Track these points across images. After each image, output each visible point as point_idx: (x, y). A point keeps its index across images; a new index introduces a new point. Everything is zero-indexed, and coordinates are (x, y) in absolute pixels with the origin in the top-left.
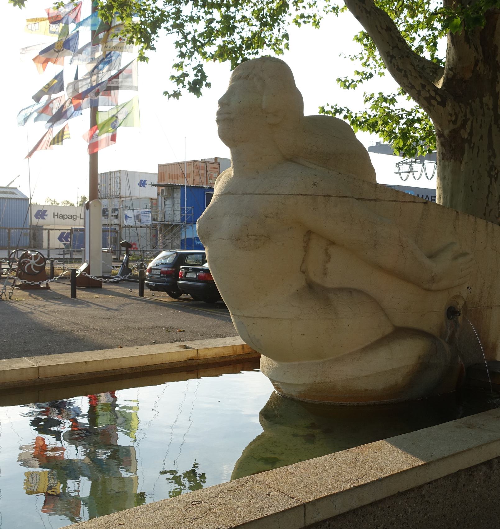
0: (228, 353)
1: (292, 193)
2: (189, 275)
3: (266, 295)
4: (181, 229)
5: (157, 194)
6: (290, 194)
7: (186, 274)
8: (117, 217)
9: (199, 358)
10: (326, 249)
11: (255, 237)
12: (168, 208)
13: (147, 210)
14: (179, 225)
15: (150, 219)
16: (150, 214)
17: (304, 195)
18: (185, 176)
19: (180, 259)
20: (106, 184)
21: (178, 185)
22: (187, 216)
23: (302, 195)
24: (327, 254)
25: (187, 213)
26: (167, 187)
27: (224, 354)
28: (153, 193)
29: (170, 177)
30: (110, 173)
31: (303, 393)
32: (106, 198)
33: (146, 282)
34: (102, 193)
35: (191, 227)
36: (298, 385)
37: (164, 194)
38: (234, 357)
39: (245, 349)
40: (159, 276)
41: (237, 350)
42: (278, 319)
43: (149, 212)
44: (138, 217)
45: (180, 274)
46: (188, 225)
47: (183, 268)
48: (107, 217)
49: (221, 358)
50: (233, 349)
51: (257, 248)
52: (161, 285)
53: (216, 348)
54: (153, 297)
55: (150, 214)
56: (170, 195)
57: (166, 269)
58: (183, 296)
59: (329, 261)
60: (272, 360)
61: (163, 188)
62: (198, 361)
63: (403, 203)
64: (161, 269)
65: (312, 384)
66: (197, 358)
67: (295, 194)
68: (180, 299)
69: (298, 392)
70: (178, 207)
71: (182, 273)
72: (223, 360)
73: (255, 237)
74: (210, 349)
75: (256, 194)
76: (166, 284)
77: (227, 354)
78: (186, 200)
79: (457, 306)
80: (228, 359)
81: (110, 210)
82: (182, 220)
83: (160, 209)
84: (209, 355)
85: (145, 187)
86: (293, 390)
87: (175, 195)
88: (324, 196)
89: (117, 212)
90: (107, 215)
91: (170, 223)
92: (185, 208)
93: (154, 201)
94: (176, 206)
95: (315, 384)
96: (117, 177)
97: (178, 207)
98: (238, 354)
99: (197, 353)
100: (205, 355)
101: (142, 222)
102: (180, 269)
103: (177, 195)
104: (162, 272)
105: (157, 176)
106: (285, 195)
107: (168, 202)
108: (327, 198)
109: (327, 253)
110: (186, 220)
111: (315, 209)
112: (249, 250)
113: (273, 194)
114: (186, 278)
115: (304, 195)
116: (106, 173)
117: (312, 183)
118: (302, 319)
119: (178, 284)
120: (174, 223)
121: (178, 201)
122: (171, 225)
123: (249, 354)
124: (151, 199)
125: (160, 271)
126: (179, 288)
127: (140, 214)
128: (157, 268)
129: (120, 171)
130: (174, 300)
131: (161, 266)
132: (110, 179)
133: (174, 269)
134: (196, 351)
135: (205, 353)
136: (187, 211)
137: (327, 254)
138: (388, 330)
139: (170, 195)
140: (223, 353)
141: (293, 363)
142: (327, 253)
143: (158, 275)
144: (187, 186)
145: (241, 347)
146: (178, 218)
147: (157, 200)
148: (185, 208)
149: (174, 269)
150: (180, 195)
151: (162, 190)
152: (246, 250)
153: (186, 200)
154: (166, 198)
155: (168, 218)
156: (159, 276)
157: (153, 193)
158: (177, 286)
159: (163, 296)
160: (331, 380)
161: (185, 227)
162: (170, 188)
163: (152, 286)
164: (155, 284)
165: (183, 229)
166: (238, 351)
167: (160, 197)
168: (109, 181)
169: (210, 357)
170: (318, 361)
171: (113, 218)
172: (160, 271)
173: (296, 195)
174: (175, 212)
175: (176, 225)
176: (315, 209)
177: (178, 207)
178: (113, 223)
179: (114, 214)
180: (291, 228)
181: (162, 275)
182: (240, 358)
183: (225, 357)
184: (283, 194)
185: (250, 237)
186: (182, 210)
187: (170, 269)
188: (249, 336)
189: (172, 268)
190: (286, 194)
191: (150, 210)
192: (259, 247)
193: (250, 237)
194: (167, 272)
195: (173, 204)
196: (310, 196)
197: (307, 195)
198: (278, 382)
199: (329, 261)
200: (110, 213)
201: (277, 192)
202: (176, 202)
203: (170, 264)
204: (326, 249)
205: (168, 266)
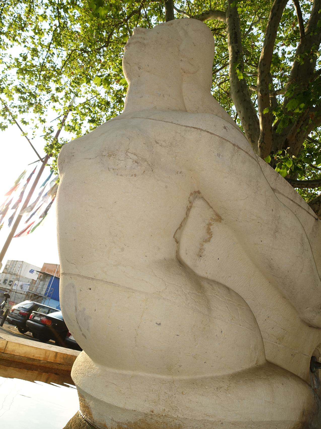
0: (38, 356)
1: (197, 127)
2: (36, 318)
3: (123, 250)
4: (43, 299)
5: (37, 278)
6: (194, 128)
7: (34, 317)
8: (10, 285)
9: (6, 352)
10: (210, 224)
11: (135, 158)
12: (40, 286)
13: (28, 283)
14: (42, 296)
15: (28, 289)
16: (29, 286)
17: (211, 133)
18: (57, 267)
19: (34, 308)
20: (12, 266)
21: (50, 275)
22: (49, 293)
23: (208, 132)
24: (209, 231)
25: (49, 291)
26: (44, 274)
27: (34, 356)
28: (35, 276)
29: (48, 270)
30: (17, 261)
31: (125, 426)
32: (9, 273)
33: (8, 317)
34: (8, 271)
35: (48, 300)
36: (124, 410)
37: (41, 278)
38: (42, 363)
39: (57, 357)
40: (17, 315)
41: (49, 356)
42: (129, 288)
43: (29, 285)
44: (21, 287)
45: (30, 317)
46: (48, 298)
47: (34, 313)
48: (5, 284)
49: (29, 359)
50: (46, 353)
51: (132, 175)
52: (16, 321)
53: (28, 346)
54: (8, 329)
55: (29, 286)
56: (44, 279)
57: (23, 312)
58: (28, 333)
59: (209, 241)
60: (92, 362)
61: (42, 274)
62: (3, 354)
63: (299, 207)
64: (20, 311)
65: (146, 414)
66: (3, 351)
67: (199, 129)
68: (25, 334)
69: (119, 423)
70: (46, 287)
71: (32, 315)
72: (30, 362)
73: (135, 158)
74: (21, 346)
75: (150, 119)
76: (19, 321)
77: (37, 357)
78: (51, 284)
79: (319, 358)
80: (36, 363)
81: (8, 281)
82: (46, 294)
83: (36, 285)
84: (17, 352)
85: (32, 273)
86: (110, 418)
87: (47, 280)
88: (234, 145)
89: (11, 283)
90: (6, 283)
91: (38, 294)
92: (50, 288)
93: (34, 282)
94: (45, 286)
95: (151, 415)
96: (20, 264)
97: (46, 286)
98: (48, 361)
99: (5, 345)
100: (14, 351)
101: (23, 289)
102: (32, 313)
103: (48, 280)
104: (20, 313)
105: (41, 269)
106: (187, 127)
107: (41, 283)
108: (236, 148)
109: (209, 229)
110: (47, 294)
111: (219, 155)
112: (121, 175)
113: (172, 123)
114: (33, 320)
115: (211, 133)
116: (15, 261)
117: (223, 126)
118: (163, 299)
119: (26, 323)
120: (40, 295)
121: (47, 283)
122: (38, 295)
123: (60, 364)
124: (33, 280)
125: (19, 312)
126: (26, 325)
127: (23, 285)
128: (18, 309)
129: (23, 262)
130: (20, 334)
131: (21, 309)
132: (16, 264)
133: (28, 313)
134: (5, 343)
135: (14, 348)
136: (50, 290)
137: (209, 231)
138: (262, 362)
139: (44, 279)
140: (33, 354)
141: (124, 372)
142: (209, 229)
143: (17, 314)
144: (55, 277)
145: (55, 354)
146: (43, 293)
147: (36, 281)
148: (50, 288)
149: (28, 313)
150: (49, 280)
151: (41, 275)
152: (117, 175)
153: (51, 284)
154: (41, 280)
155: (38, 292)
156: (17, 315)
157: (35, 276)
158: (26, 324)
159: (15, 329)
160: (179, 415)
161: (45, 298)
162: (45, 275)
163: (10, 320)
164: (13, 320)
165: (44, 300)
166: (49, 358)
167: (38, 280)
168: (15, 265)
169: (18, 354)
170: (164, 377)
171: (8, 285)
172: (19, 312)
173: (201, 130)
174: (43, 289)
175: (41, 297)
176: (219, 155)
177: (46, 286)
178: (7, 288)
179: (10, 283)
180: (181, 173)
181: (19, 315)
182: (49, 365)
183: (34, 360)
184: (185, 126)
185: (129, 154)
186: (48, 289)
187: (26, 312)
188: (76, 310)
189: (27, 312)
190: (189, 127)
191: (30, 284)
192: (135, 175)
193: (129, 154)
194: (23, 313)
195: (44, 285)
196: (217, 137)
197: (214, 134)
198: (92, 398)
199: (207, 240)
200: (8, 282)
201: (177, 123)
202: (46, 284)
203: (27, 309)
204: (210, 224)
205: (26, 310)
